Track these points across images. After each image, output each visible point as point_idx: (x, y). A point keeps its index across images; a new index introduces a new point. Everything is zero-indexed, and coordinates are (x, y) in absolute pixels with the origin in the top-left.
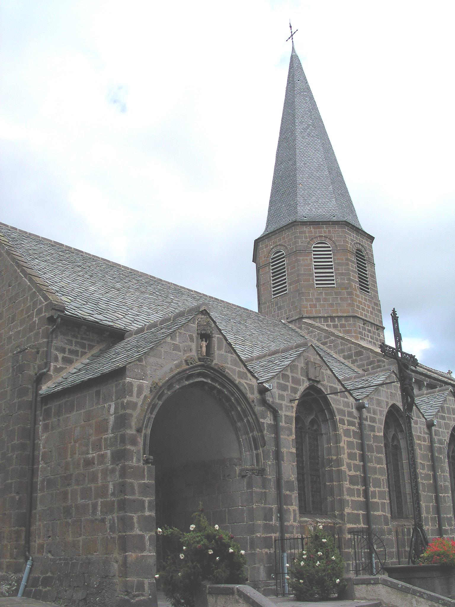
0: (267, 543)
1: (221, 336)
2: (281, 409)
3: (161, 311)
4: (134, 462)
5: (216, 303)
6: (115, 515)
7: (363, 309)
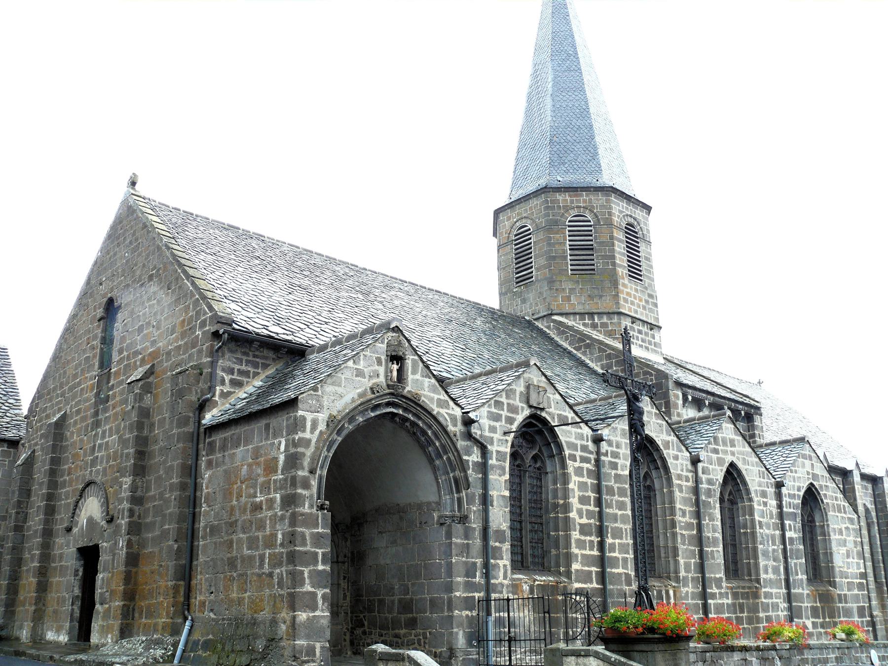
0: (468, 603)
1: (416, 358)
2: (492, 444)
4: (306, 509)
6: (283, 569)
7: (632, 303)
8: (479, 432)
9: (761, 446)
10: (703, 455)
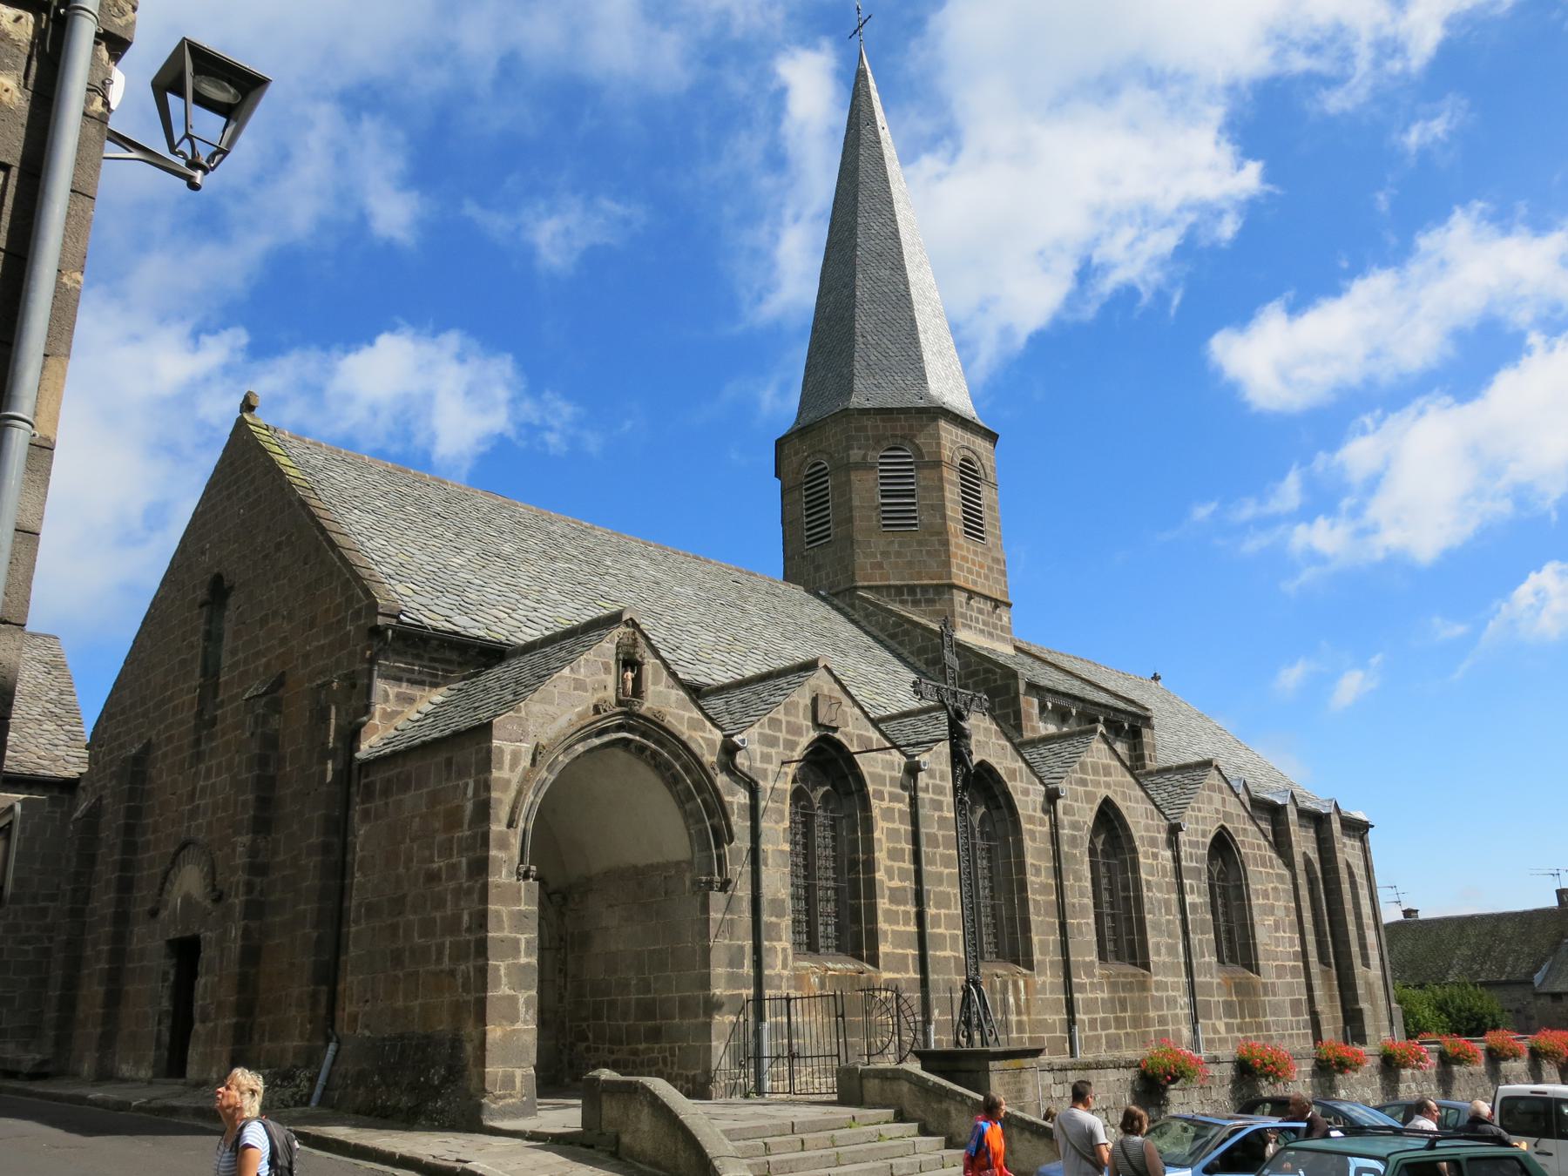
2: (765, 778)
6: (471, 965)
8: (747, 763)
9: (1150, 773)
10: (1063, 787)
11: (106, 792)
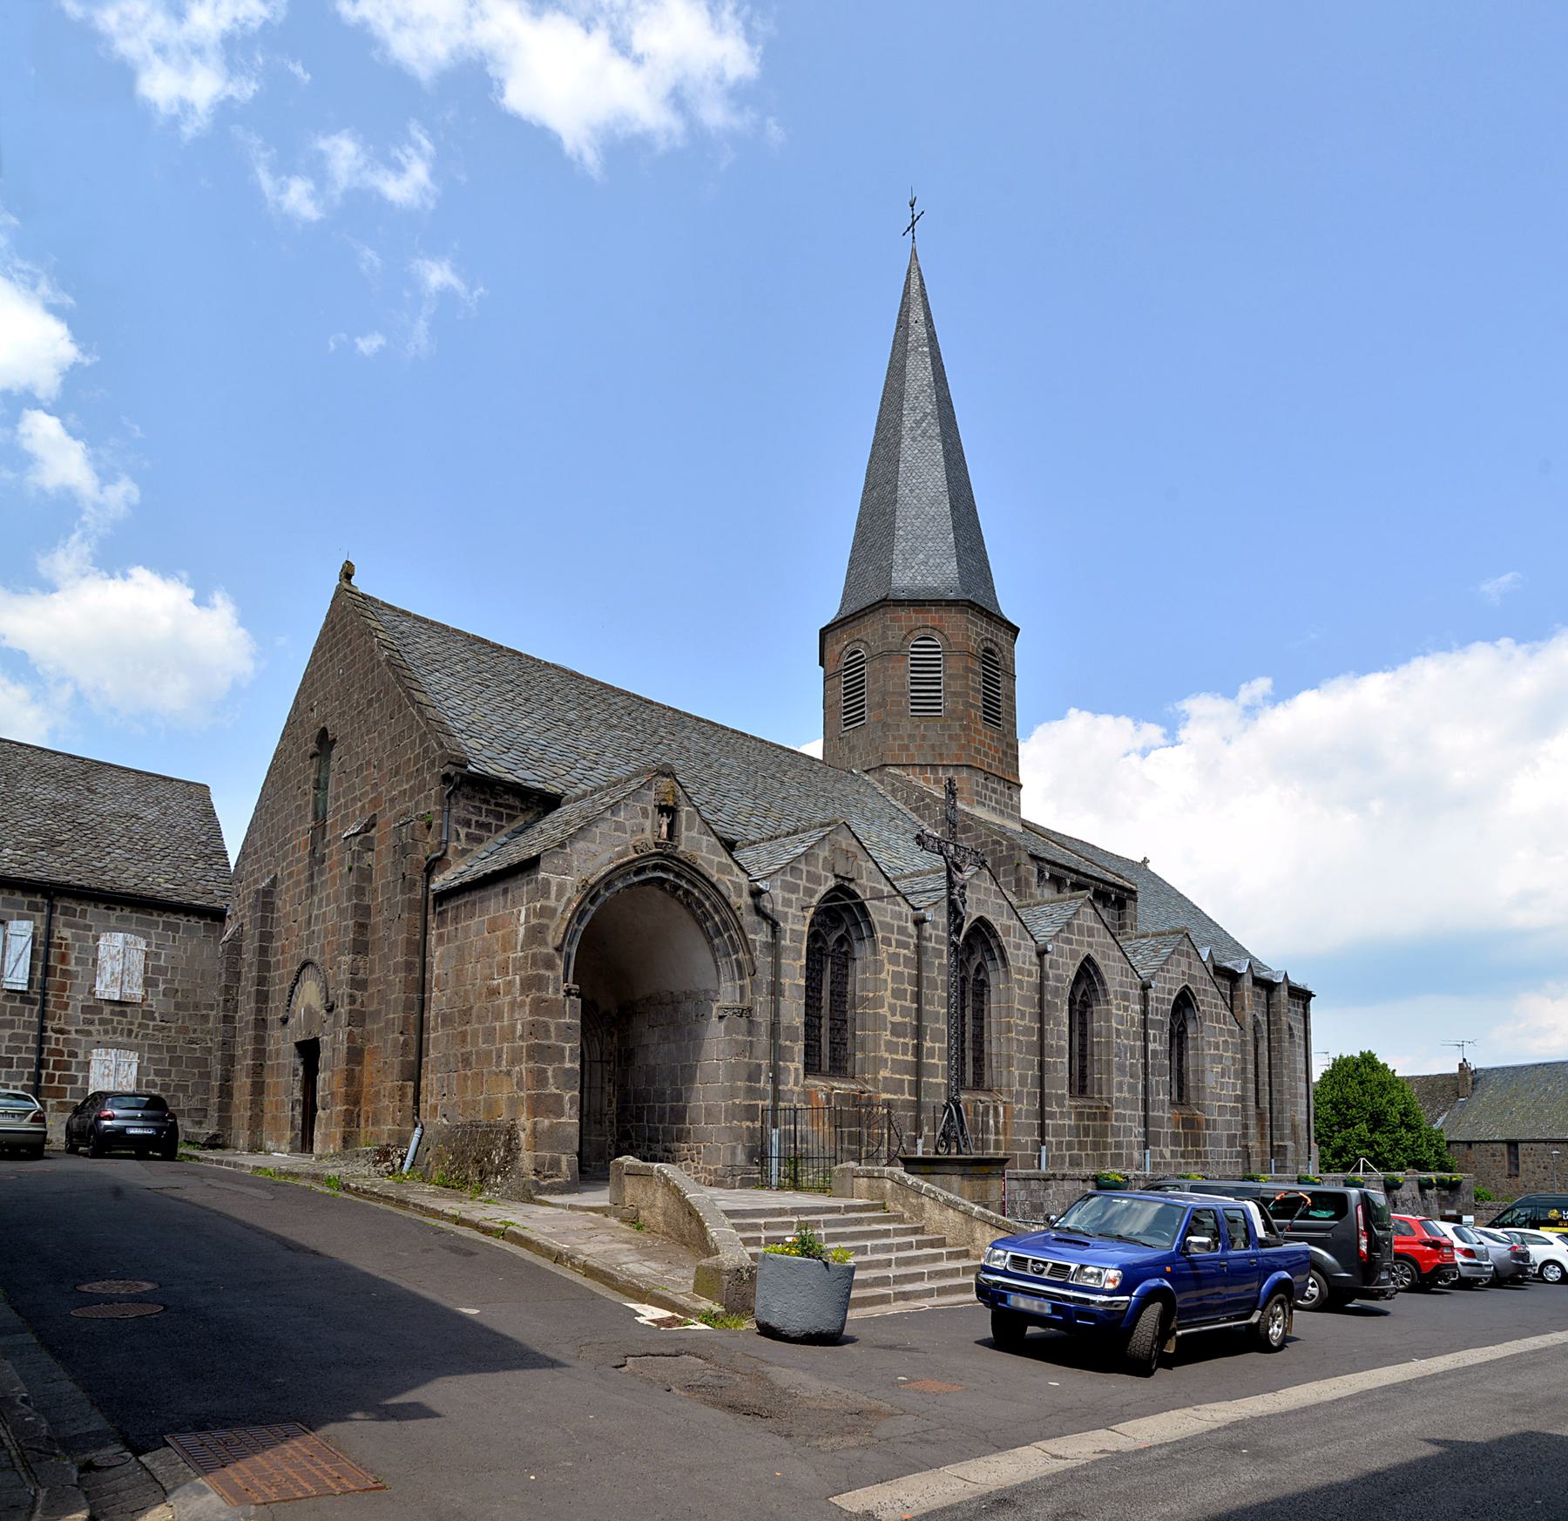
2: (786, 921)
3: (636, 760)
4: (550, 994)
5: (742, 741)
7: (986, 755)
11: (246, 920)
